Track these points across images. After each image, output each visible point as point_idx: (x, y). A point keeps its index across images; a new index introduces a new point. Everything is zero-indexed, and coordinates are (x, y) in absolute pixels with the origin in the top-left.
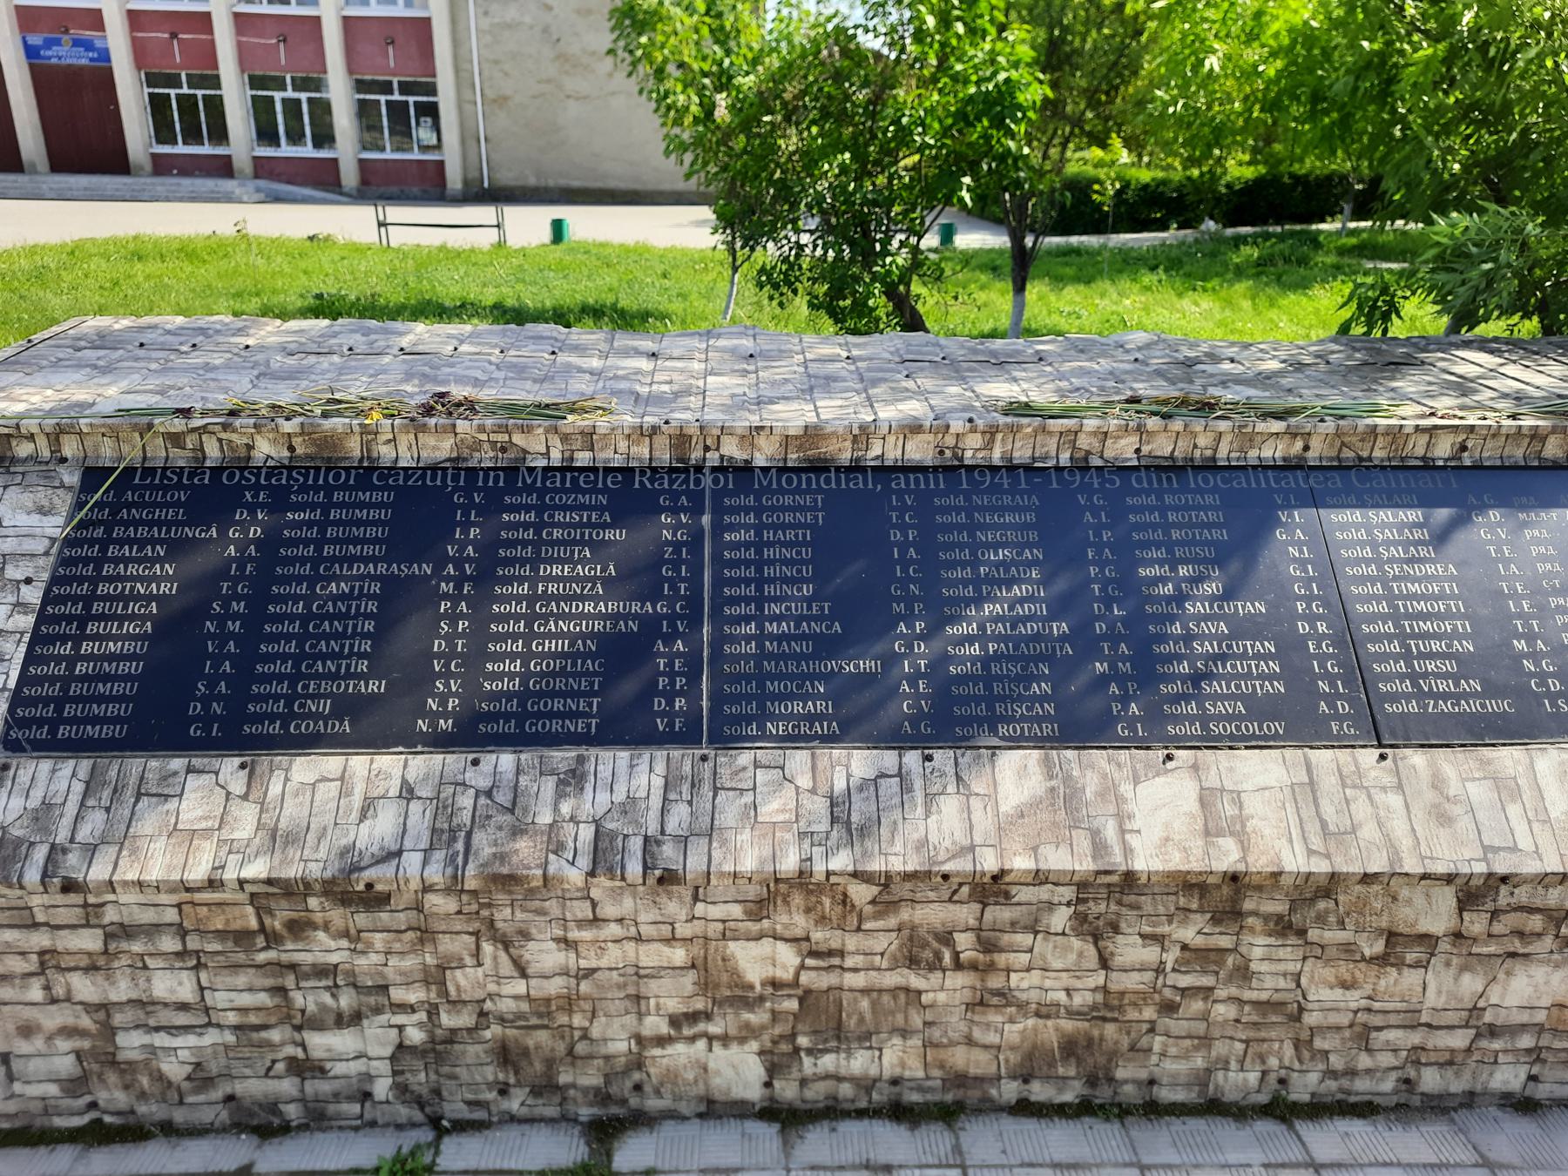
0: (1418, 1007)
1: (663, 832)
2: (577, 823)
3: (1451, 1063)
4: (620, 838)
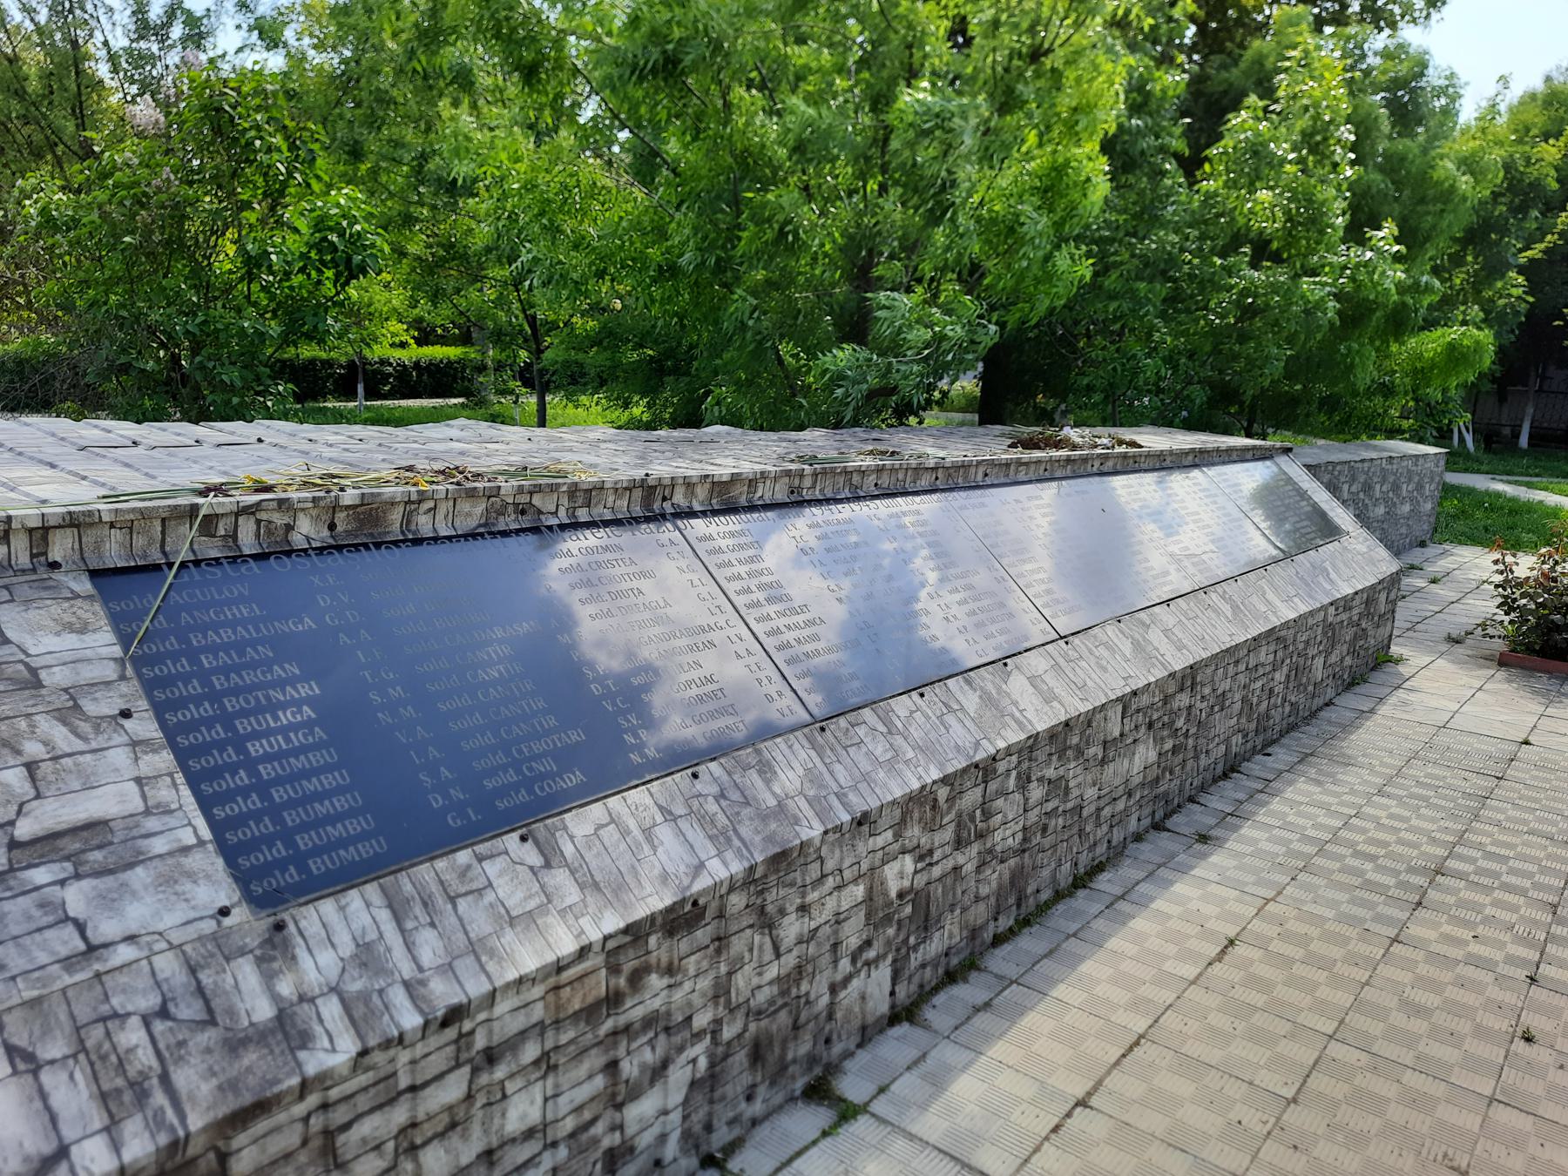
0: (389, 1069)
1: (421, 969)
2: (312, 1000)
3: (453, 1126)
4: (375, 998)
